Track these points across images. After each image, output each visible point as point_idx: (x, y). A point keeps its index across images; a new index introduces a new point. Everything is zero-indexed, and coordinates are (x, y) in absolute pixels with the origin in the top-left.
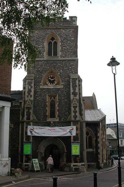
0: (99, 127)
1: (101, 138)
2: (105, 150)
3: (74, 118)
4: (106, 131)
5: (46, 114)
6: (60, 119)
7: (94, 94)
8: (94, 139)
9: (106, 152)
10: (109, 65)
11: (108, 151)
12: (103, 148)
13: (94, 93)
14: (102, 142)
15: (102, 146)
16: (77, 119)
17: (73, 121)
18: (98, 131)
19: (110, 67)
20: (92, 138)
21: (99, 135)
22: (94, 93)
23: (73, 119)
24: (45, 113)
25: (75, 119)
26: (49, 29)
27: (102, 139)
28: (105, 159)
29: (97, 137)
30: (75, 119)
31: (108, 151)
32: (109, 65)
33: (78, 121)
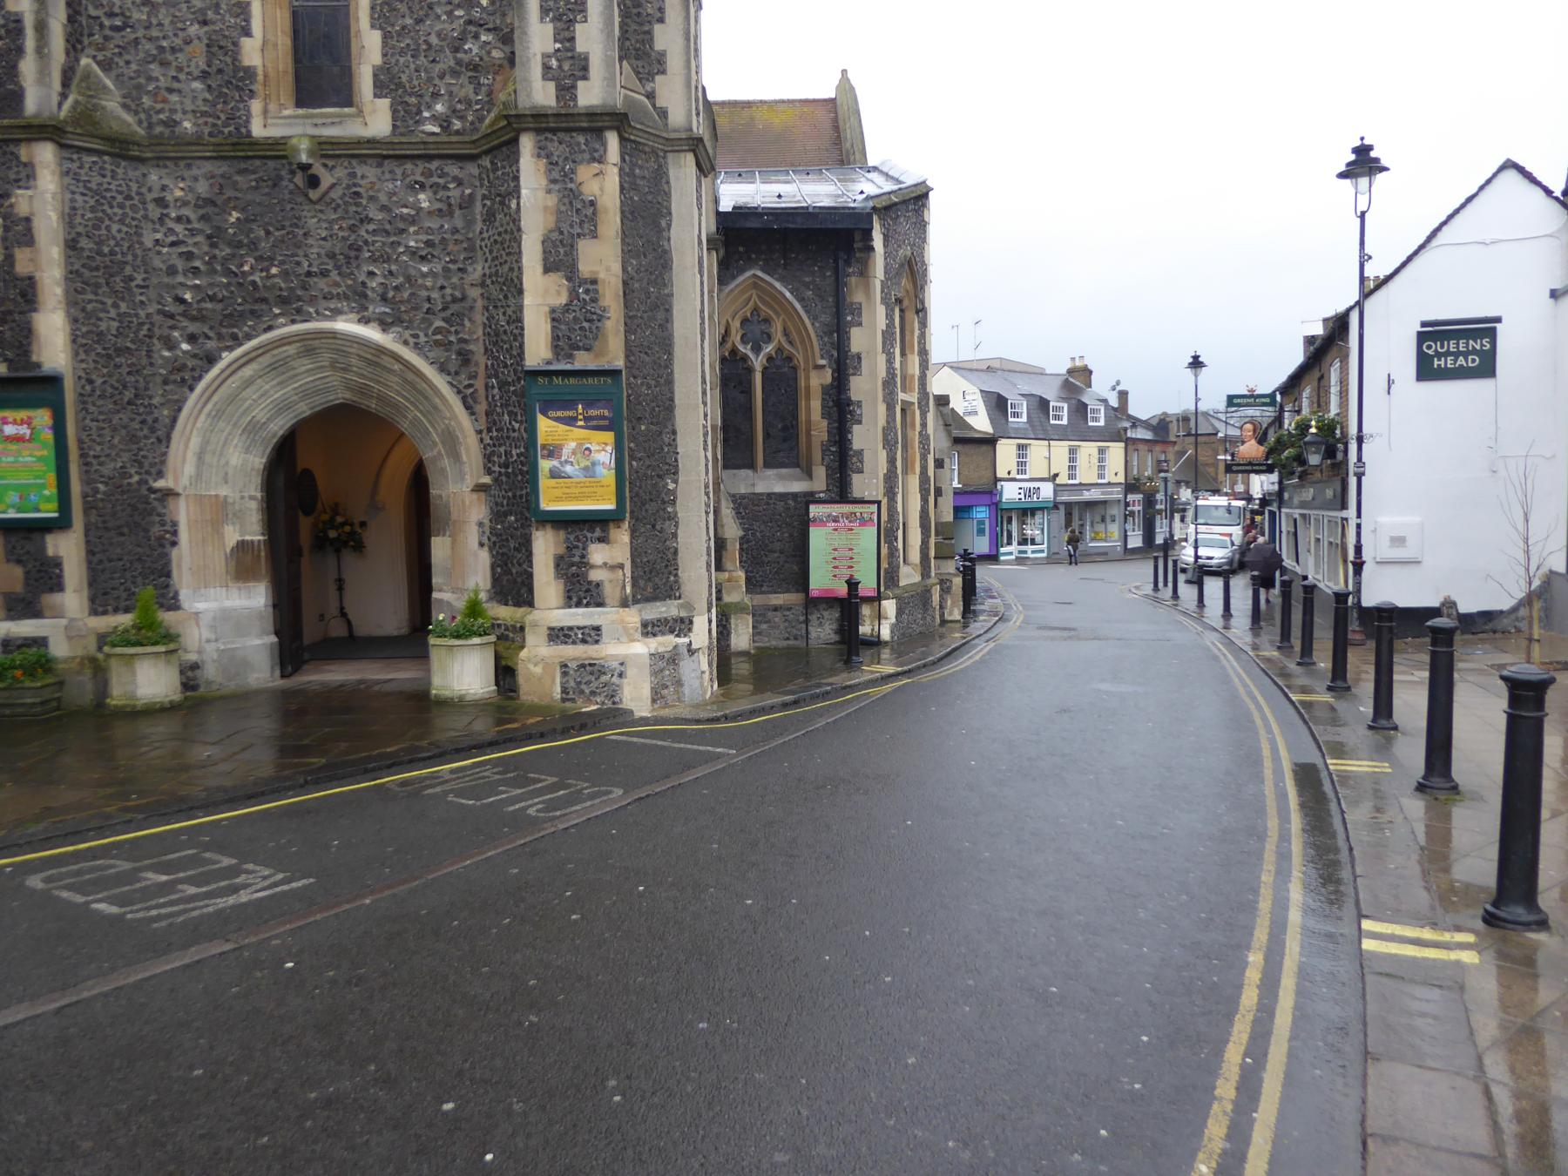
0: (864, 273)
1: (883, 374)
2: (914, 482)
3: (551, 86)
4: (924, 324)
5: (234, 51)
6: (404, 115)
7: (845, 85)
8: (818, 380)
9: (925, 500)
10: (1342, 175)
11: (938, 492)
12: (892, 461)
13: (844, 72)
14: (890, 408)
15: (889, 444)
16: (590, 95)
17: (542, 123)
18: (857, 311)
19: (1347, 182)
20: (795, 369)
21: (858, 340)
22: (844, 72)
23: (542, 94)
24: (223, 47)
25: (566, 91)
26: (238, 387)
27: (889, 383)
28: (915, 555)
29: (844, 365)
30: (566, 91)
31: (938, 492)
32: (1342, 175)
33: (598, 122)
